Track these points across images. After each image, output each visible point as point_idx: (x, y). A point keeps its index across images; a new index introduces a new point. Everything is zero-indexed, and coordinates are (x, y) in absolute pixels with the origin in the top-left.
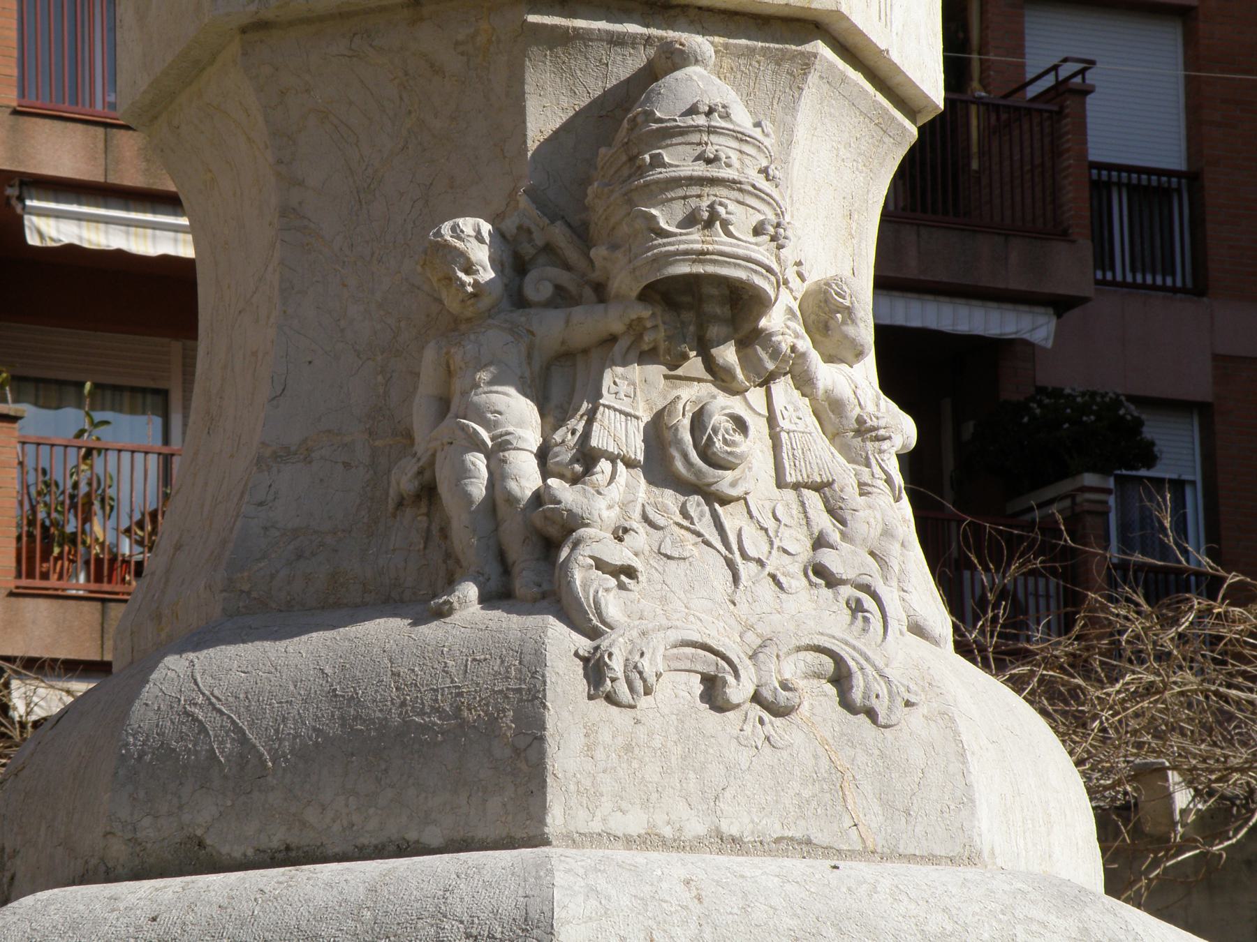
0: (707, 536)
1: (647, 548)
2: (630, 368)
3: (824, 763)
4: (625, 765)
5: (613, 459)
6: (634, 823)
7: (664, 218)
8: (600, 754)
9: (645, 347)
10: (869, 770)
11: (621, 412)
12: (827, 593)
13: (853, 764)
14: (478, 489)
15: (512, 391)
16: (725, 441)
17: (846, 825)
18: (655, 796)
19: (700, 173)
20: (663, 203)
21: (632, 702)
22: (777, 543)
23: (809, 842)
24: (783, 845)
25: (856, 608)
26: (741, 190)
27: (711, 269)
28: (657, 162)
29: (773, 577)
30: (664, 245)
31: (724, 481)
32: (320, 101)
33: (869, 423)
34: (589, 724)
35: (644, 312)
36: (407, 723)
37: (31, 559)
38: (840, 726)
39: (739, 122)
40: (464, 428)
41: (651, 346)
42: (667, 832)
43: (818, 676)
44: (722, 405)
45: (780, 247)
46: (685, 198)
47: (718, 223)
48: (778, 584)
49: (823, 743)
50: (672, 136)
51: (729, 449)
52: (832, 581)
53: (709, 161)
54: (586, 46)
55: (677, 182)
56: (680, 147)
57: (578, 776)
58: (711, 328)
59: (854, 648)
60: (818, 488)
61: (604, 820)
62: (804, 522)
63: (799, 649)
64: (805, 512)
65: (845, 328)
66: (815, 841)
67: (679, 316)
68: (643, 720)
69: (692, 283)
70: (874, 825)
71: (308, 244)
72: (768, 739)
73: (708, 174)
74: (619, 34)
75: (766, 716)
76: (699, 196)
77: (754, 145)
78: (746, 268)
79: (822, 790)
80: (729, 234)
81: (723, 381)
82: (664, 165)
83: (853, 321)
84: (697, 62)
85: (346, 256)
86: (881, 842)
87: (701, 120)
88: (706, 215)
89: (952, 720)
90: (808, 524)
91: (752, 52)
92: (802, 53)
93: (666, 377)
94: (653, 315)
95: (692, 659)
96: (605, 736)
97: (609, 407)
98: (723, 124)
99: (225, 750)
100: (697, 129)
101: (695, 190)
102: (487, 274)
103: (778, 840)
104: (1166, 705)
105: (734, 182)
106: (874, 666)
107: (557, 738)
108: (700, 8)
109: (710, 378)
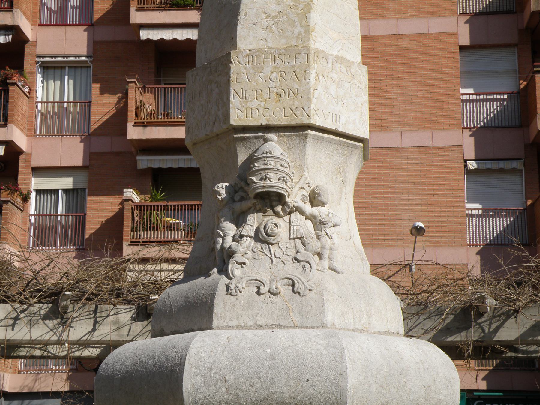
0: (266, 253)
1: (251, 257)
2: (254, 214)
3: (285, 306)
4: (233, 310)
5: (247, 236)
6: (235, 323)
7: (254, 179)
8: (227, 307)
9: (258, 209)
11: (250, 225)
12: (298, 264)
14: (219, 246)
15: (228, 222)
16: (271, 230)
17: (290, 320)
18: (240, 316)
21: (236, 295)
22: (285, 253)
23: (280, 325)
24: (273, 326)
25: (304, 267)
26: (274, 170)
27: (267, 190)
28: (254, 166)
29: (283, 262)
30: (255, 185)
31: (272, 240)
33: (322, 221)
36: (195, 302)
39: (275, 154)
40: (218, 232)
42: (243, 325)
43: (288, 285)
44: (276, 220)
45: (286, 182)
46: (260, 174)
47: (268, 179)
48: (284, 263)
49: (286, 301)
50: (258, 159)
51: (271, 232)
52: (299, 261)
53: (266, 164)
54: (250, 140)
55: (258, 170)
60: (300, 238)
61: (227, 323)
62: (295, 247)
63: (283, 279)
64: (295, 245)
65: (318, 198)
66: (281, 325)
69: (268, 193)
70: (297, 320)
72: (271, 301)
73: (265, 168)
74: (257, 136)
75: (271, 296)
76: (264, 173)
77: (279, 159)
78: (275, 188)
79: (284, 313)
80: (271, 181)
81: (278, 215)
82: (255, 167)
83: (320, 196)
84: (270, 141)
86: (299, 324)
87: (265, 155)
88: (264, 177)
89: (322, 293)
90: (296, 248)
91: (291, 135)
92: (304, 134)
93: (263, 216)
94: (257, 201)
95: (254, 283)
96: (229, 303)
97: (248, 224)
98: (270, 155)
99: (168, 309)
100: (264, 157)
101: (263, 172)
102: (224, 196)
103: (271, 325)
104: (28, 303)
105: (272, 168)
106: (302, 282)
107: (217, 304)
108: (278, 127)
109: (274, 215)
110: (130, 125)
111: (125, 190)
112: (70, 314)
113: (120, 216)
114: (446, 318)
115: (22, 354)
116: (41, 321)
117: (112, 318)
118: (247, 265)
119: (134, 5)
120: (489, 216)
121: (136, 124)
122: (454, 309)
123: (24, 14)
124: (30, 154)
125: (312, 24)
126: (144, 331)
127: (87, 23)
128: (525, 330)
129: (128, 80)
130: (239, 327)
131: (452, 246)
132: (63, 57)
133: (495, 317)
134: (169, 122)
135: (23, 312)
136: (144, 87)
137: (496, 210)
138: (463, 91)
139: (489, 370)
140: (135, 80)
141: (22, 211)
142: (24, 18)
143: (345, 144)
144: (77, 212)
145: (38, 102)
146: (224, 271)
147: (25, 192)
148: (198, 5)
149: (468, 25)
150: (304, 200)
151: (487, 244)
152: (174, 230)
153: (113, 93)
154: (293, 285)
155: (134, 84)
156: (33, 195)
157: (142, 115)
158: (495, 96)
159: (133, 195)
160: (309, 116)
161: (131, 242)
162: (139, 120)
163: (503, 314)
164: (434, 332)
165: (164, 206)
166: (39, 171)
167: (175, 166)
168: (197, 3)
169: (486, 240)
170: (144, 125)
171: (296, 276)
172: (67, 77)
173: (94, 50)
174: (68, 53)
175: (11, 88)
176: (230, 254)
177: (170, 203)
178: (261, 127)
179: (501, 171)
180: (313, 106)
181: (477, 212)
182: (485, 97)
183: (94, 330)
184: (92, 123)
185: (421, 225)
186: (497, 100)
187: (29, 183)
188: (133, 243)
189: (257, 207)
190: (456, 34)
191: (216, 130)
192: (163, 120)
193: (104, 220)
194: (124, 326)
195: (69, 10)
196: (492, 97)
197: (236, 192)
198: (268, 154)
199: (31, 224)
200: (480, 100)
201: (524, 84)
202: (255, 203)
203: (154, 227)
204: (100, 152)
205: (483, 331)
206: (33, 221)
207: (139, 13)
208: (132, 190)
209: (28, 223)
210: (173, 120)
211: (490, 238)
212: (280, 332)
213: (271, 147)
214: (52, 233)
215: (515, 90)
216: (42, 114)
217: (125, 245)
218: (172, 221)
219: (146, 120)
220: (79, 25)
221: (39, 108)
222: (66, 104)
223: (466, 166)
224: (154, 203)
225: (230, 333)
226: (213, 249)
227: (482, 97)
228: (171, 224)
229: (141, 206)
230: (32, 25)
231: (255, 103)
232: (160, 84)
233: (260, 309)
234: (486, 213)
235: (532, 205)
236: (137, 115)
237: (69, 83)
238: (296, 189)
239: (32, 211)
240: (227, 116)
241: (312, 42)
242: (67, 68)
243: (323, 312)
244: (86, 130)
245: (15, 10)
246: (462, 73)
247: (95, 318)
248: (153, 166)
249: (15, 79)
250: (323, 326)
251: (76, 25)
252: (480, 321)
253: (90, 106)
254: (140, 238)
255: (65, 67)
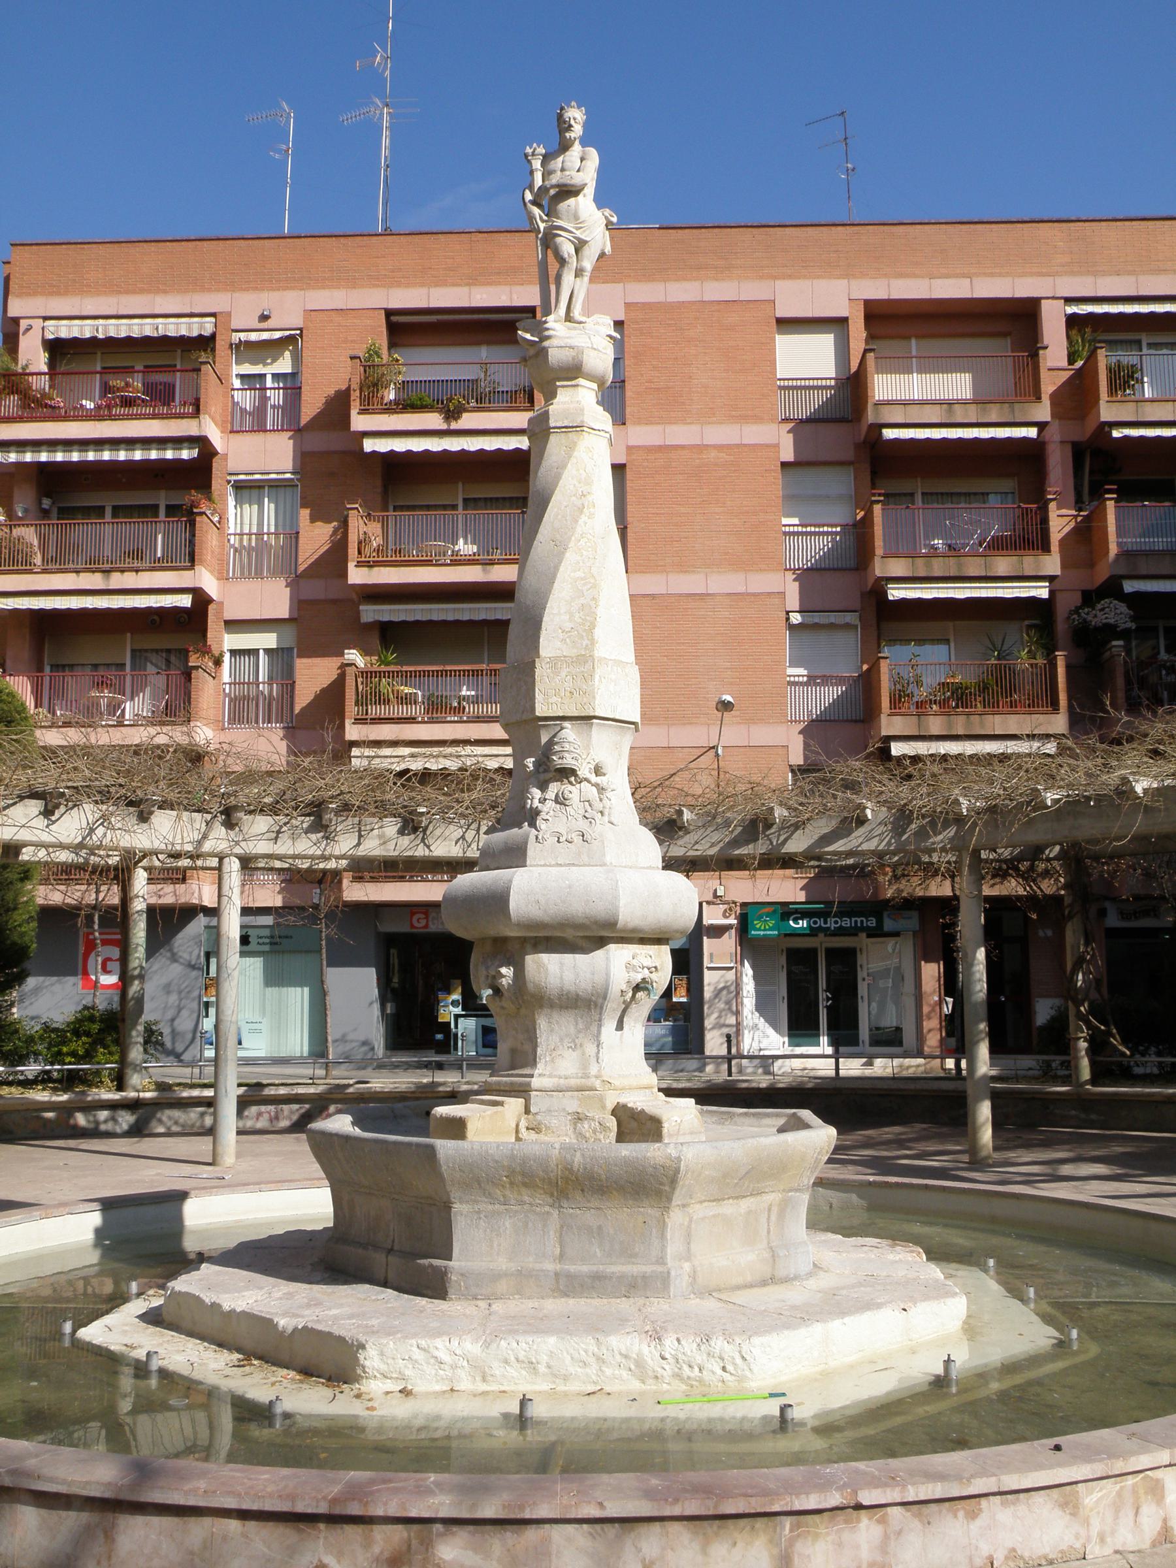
6: (542, 863)
7: (554, 758)
14: (528, 806)
31: (567, 802)
37: (895, 703)
44: (570, 787)
99: (491, 851)
110: (351, 566)
111: (346, 651)
112: (333, 828)
113: (339, 684)
114: (733, 831)
115: (261, 865)
116: (303, 835)
117: (376, 832)
119: (355, 406)
120: (816, 684)
121: (359, 564)
122: (743, 820)
123: (213, 419)
124: (222, 603)
125: (596, 638)
126: (411, 845)
127: (292, 427)
128: (813, 841)
129: (348, 506)
130: (545, 865)
131: (769, 723)
132: (262, 473)
133: (783, 828)
134: (402, 561)
135: (285, 824)
136: (369, 514)
137: (825, 676)
138: (785, 521)
139: (807, 878)
140: (357, 506)
141: (214, 678)
142: (213, 425)
143: (621, 727)
144: (282, 680)
145: (230, 534)
146: (533, 824)
147: (217, 654)
148: (440, 406)
149: (791, 435)
151: (813, 721)
152: (411, 704)
153: (329, 521)
154: (583, 836)
155: (356, 511)
156: (227, 658)
157: (367, 551)
158: (826, 529)
159: (358, 659)
161: (355, 719)
162: (363, 559)
163: (791, 825)
164: (721, 844)
165: (397, 672)
166: (234, 625)
167: (410, 618)
168: (438, 403)
169: (812, 714)
170: (369, 565)
172: (266, 500)
173: (303, 465)
174: (267, 469)
175: (198, 519)
176: (536, 813)
177: (405, 668)
179: (832, 627)
180: (597, 702)
181: (801, 679)
182: (813, 529)
183: (359, 844)
184: (300, 561)
185: (728, 698)
186: (827, 533)
187: (221, 642)
188: (358, 721)
190: (777, 446)
191: (524, 717)
192: (394, 558)
193: (318, 690)
194: (390, 840)
195: (269, 411)
196: (821, 530)
197: (540, 765)
198: (564, 739)
199: (225, 695)
200: (807, 534)
201: (861, 514)
203: (384, 700)
204: (311, 601)
205: (771, 843)
206: (227, 691)
207: (362, 416)
208: (355, 651)
209: (222, 693)
210: (406, 558)
211: (816, 712)
212: (574, 868)
214: (253, 705)
215: (850, 522)
216: (236, 550)
217: (348, 723)
218: (407, 690)
219: (371, 559)
220: (282, 430)
221: (232, 542)
222: (266, 536)
223: (788, 619)
224: (383, 668)
225: (540, 869)
226: (524, 807)
227: (808, 529)
228: (406, 694)
229: (367, 672)
230: (222, 432)
231: (554, 699)
232: (388, 511)
234: (812, 680)
235: (869, 670)
236: (360, 553)
237: (269, 508)
238: (584, 765)
239: (226, 678)
240: (533, 709)
241: (596, 652)
242: (266, 488)
243: (604, 855)
244: (293, 571)
245: (202, 416)
246: (784, 496)
247: (360, 831)
248: (381, 619)
249: (204, 507)
250: (604, 865)
251: (278, 430)
252: (767, 833)
253: (297, 538)
254: (367, 714)
255: (263, 487)
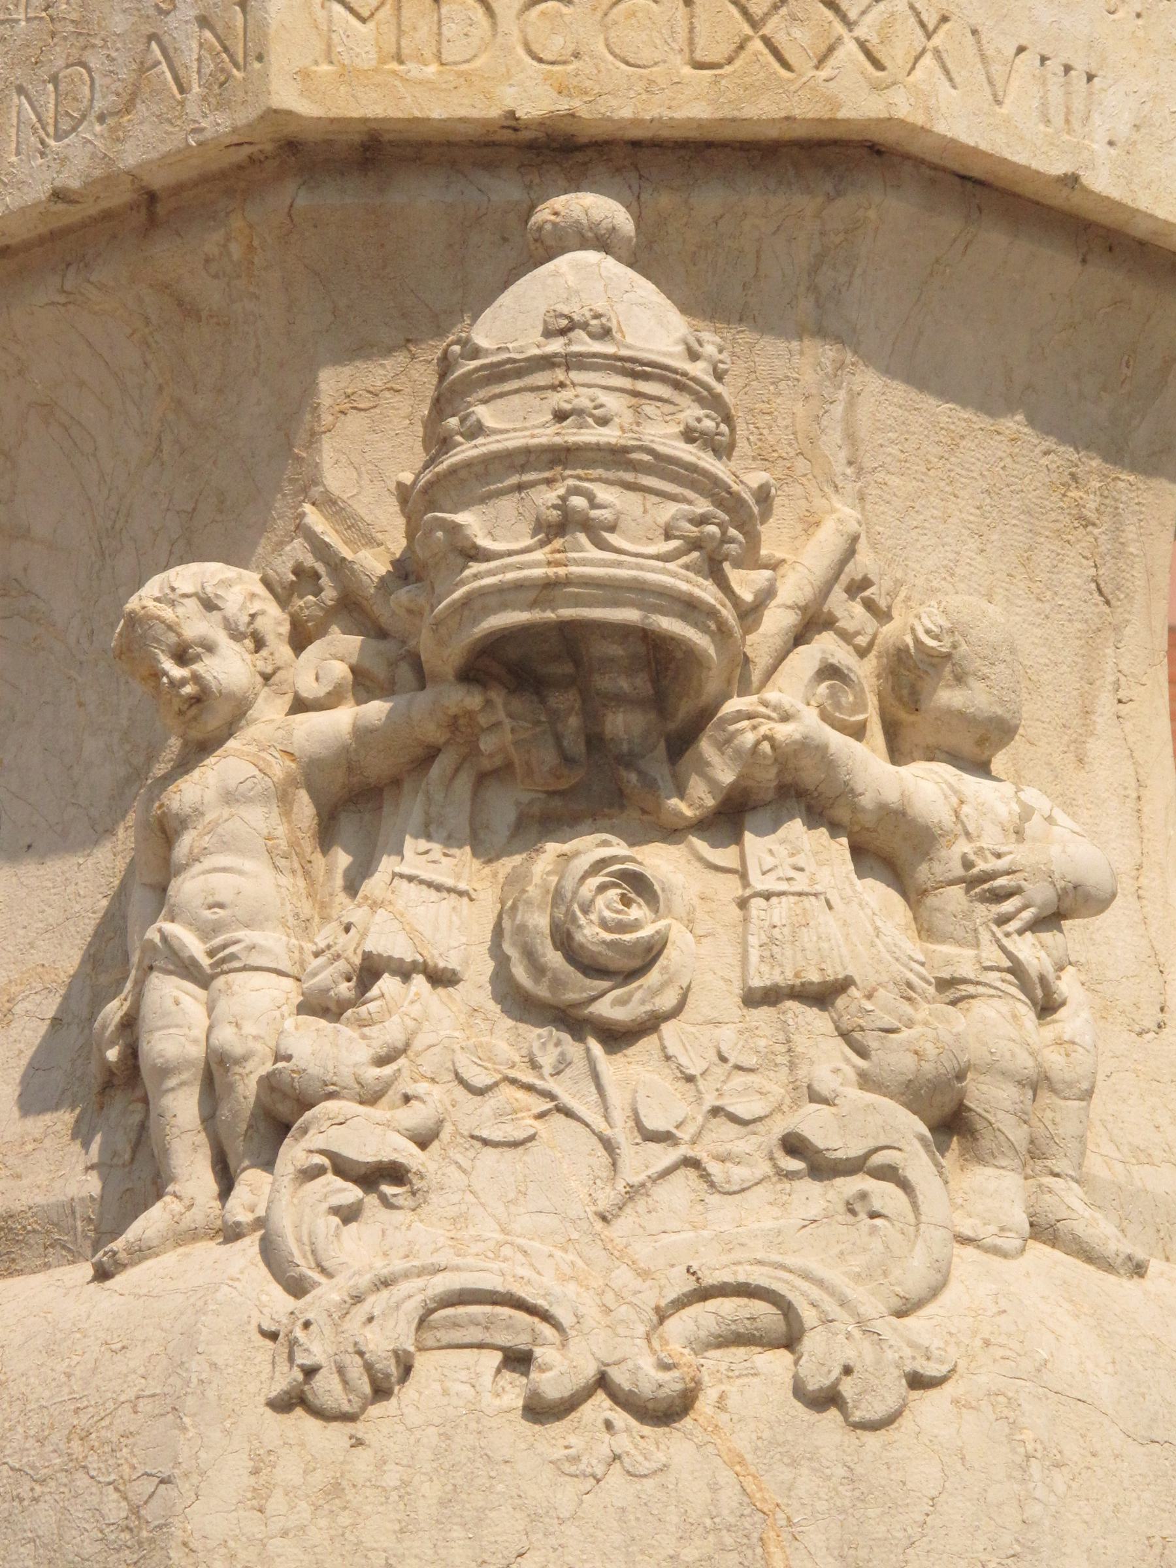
3: (730, 1497)
5: (405, 972)
8: (277, 1503)
10: (821, 1506)
13: (789, 1497)
19: (544, 440)
20: (484, 499)
30: (476, 576)
32: (39, 387)
33: (981, 866)
34: (261, 1452)
35: (473, 700)
38: (771, 1428)
39: (629, 340)
41: (498, 761)
56: (516, 399)
57: (231, 1544)
58: (610, 717)
59: (820, 1283)
67: (543, 701)
68: (368, 1438)
71: (35, 639)
85: (85, 653)
94: (488, 703)
95: (488, 1325)
96: (288, 1471)
108: (636, 144)
118: (417, 1184)
150: (838, 706)
160: (878, 65)
171: (806, 1276)
178: (508, 135)
189: (487, 744)
202: (470, 715)
213: (600, 286)
233: (534, 1518)
